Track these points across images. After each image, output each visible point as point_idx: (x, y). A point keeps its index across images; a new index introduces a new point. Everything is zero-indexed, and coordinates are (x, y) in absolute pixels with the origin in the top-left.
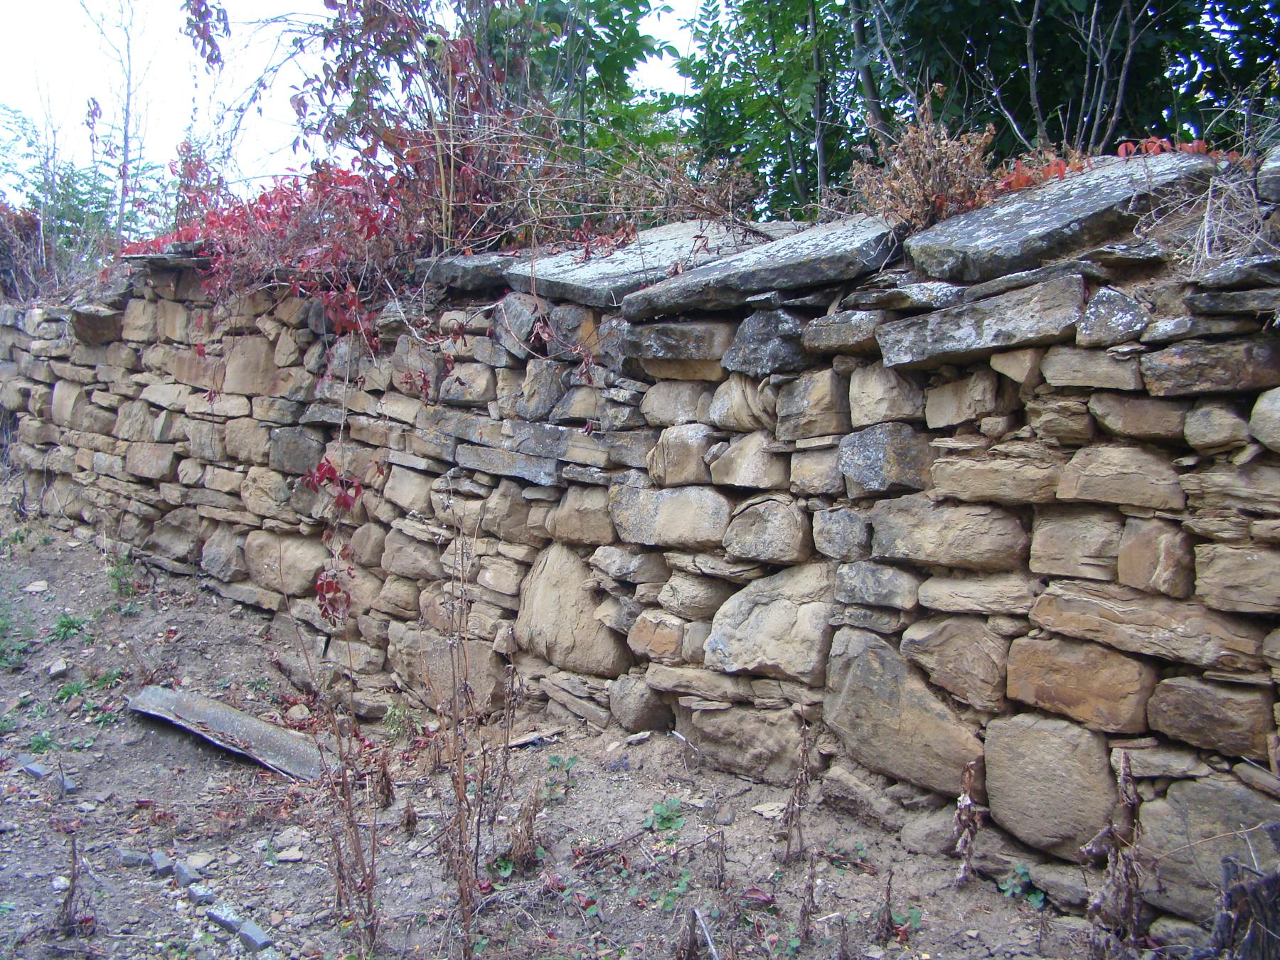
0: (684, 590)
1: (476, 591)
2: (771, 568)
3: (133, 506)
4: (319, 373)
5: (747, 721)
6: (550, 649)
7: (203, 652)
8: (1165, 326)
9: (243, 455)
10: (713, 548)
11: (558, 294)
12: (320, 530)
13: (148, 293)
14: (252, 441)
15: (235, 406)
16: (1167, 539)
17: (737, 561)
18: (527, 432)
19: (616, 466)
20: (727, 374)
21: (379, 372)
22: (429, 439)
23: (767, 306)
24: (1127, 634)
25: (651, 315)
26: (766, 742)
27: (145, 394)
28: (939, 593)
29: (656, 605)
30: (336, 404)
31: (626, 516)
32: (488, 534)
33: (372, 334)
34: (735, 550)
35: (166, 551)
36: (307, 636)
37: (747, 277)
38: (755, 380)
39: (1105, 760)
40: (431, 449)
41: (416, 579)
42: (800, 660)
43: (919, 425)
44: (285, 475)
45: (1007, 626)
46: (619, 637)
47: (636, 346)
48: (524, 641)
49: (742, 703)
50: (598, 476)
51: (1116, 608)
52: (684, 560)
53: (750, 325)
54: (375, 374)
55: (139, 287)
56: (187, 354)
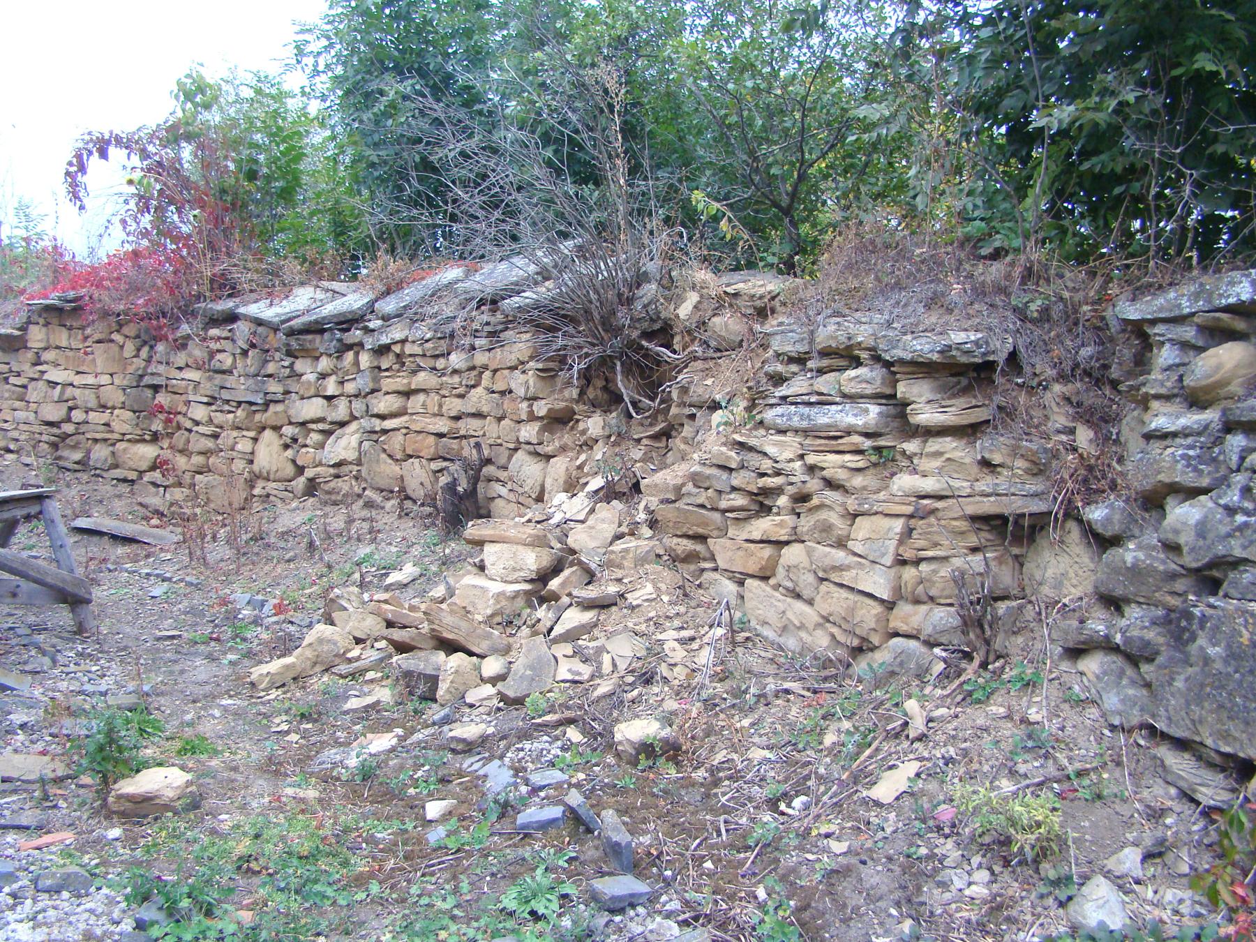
0: (315, 437)
1: (235, 454)
2: (342, 424)
3: (45, 438)
4: (149, 361)
5: (338, 483)
6: (268, 473)
7: (101, 502)
8: (428, 336)
9: (110, 404)
10: (321, 420)
11: (259, 322)
12: (155, 438)
13: (41, 321)
14: (117, 397)
15: (105, 379)
16: (437, 397)
17: (332, 423)
18: (251, 381)
19: (287, 392)
20: (322, 354)
21: (181, 358)
22: (208, 388)
23: (330, 329)
24: (432, 429)
25: (291, 333)
26: (346, 488)
27: (46, 377)
28: (388, 424)
29: (306, 446)
30: (159, 375)
31: (292, 412)
32: (238, 428)
33: (175, 340)
34: (329, 419)
35: (67, 459)
36: (153, 490)
37: (324, 318)
38: (330, 355)
39: (627, 537)
40: (209, 393)
41: (205, 453)
42: (351, 455)
43: (379, 368)
44: (134, 412)
45: (404, 431)
46: (294, 462)
47: (288, 345)
48: (257, 472)
49: (337, 476)
50: (280, 397)
51: (428, 420)
52: (313, 426)
53: (327, 336)
54: (178, 359)
55: (35, 318)
56: (71, 354)
